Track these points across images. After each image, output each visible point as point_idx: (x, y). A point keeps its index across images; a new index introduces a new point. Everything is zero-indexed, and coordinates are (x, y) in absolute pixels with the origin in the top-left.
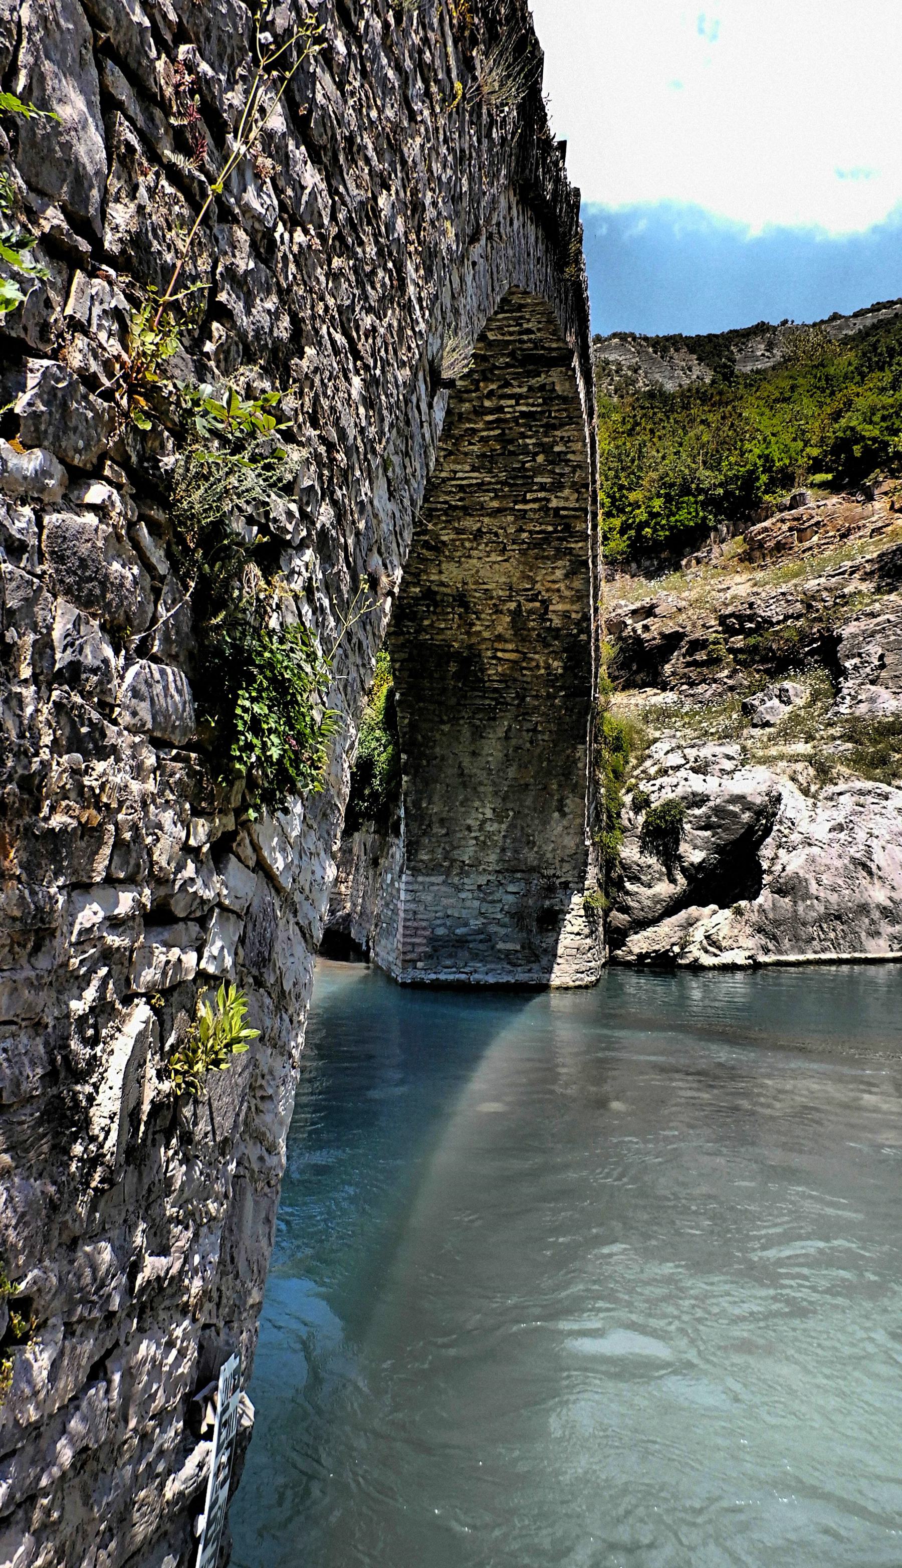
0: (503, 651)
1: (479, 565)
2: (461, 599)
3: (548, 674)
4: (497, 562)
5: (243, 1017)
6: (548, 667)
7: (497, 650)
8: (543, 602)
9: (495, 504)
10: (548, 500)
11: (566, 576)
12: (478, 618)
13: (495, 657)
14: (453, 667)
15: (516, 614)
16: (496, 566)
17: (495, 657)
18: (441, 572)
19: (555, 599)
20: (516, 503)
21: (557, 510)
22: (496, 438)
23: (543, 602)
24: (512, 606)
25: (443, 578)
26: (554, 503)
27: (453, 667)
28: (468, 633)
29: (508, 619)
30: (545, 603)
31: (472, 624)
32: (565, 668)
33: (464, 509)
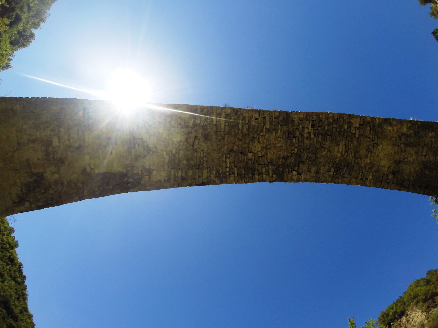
0: (422, 152)
1: (382, 153)
2: (398, 162)
3: (435, 138)
4: (382, 147)
5: (273, 171)
6: (431, 137)
7: (422, 155)
8: (402, 135)
9: (355, 143)
10: (356, 127)
11: (391, 126)
12: (407, 158)
13: (425, 156)
14: (427, 172)
15: (406, 145)
16: (384, 148)
17: (425, 156)
18: (384, 166)
19: (401, 131)
20: (355, 137)
21: (360, 124)
22: (346, 168)
23: (402, 135)
24: (402, 146)
25: (387, 166)
26: (358, 125)
27: (427, 172)
28: (413, 163)
29: (409, 148)
30: (403, 134)
31: (410, 162)
32: (432, 131)
33: (355, 152)
